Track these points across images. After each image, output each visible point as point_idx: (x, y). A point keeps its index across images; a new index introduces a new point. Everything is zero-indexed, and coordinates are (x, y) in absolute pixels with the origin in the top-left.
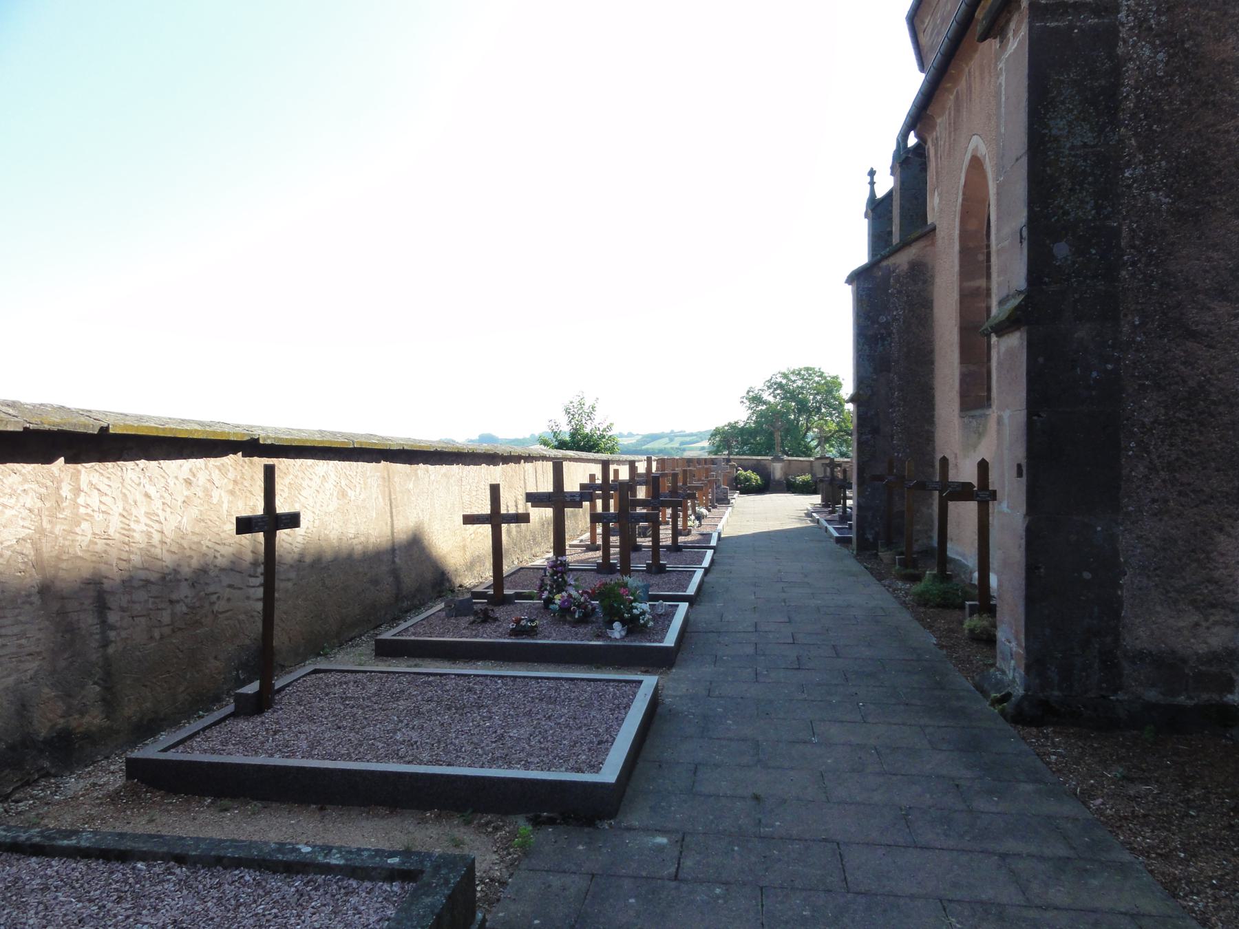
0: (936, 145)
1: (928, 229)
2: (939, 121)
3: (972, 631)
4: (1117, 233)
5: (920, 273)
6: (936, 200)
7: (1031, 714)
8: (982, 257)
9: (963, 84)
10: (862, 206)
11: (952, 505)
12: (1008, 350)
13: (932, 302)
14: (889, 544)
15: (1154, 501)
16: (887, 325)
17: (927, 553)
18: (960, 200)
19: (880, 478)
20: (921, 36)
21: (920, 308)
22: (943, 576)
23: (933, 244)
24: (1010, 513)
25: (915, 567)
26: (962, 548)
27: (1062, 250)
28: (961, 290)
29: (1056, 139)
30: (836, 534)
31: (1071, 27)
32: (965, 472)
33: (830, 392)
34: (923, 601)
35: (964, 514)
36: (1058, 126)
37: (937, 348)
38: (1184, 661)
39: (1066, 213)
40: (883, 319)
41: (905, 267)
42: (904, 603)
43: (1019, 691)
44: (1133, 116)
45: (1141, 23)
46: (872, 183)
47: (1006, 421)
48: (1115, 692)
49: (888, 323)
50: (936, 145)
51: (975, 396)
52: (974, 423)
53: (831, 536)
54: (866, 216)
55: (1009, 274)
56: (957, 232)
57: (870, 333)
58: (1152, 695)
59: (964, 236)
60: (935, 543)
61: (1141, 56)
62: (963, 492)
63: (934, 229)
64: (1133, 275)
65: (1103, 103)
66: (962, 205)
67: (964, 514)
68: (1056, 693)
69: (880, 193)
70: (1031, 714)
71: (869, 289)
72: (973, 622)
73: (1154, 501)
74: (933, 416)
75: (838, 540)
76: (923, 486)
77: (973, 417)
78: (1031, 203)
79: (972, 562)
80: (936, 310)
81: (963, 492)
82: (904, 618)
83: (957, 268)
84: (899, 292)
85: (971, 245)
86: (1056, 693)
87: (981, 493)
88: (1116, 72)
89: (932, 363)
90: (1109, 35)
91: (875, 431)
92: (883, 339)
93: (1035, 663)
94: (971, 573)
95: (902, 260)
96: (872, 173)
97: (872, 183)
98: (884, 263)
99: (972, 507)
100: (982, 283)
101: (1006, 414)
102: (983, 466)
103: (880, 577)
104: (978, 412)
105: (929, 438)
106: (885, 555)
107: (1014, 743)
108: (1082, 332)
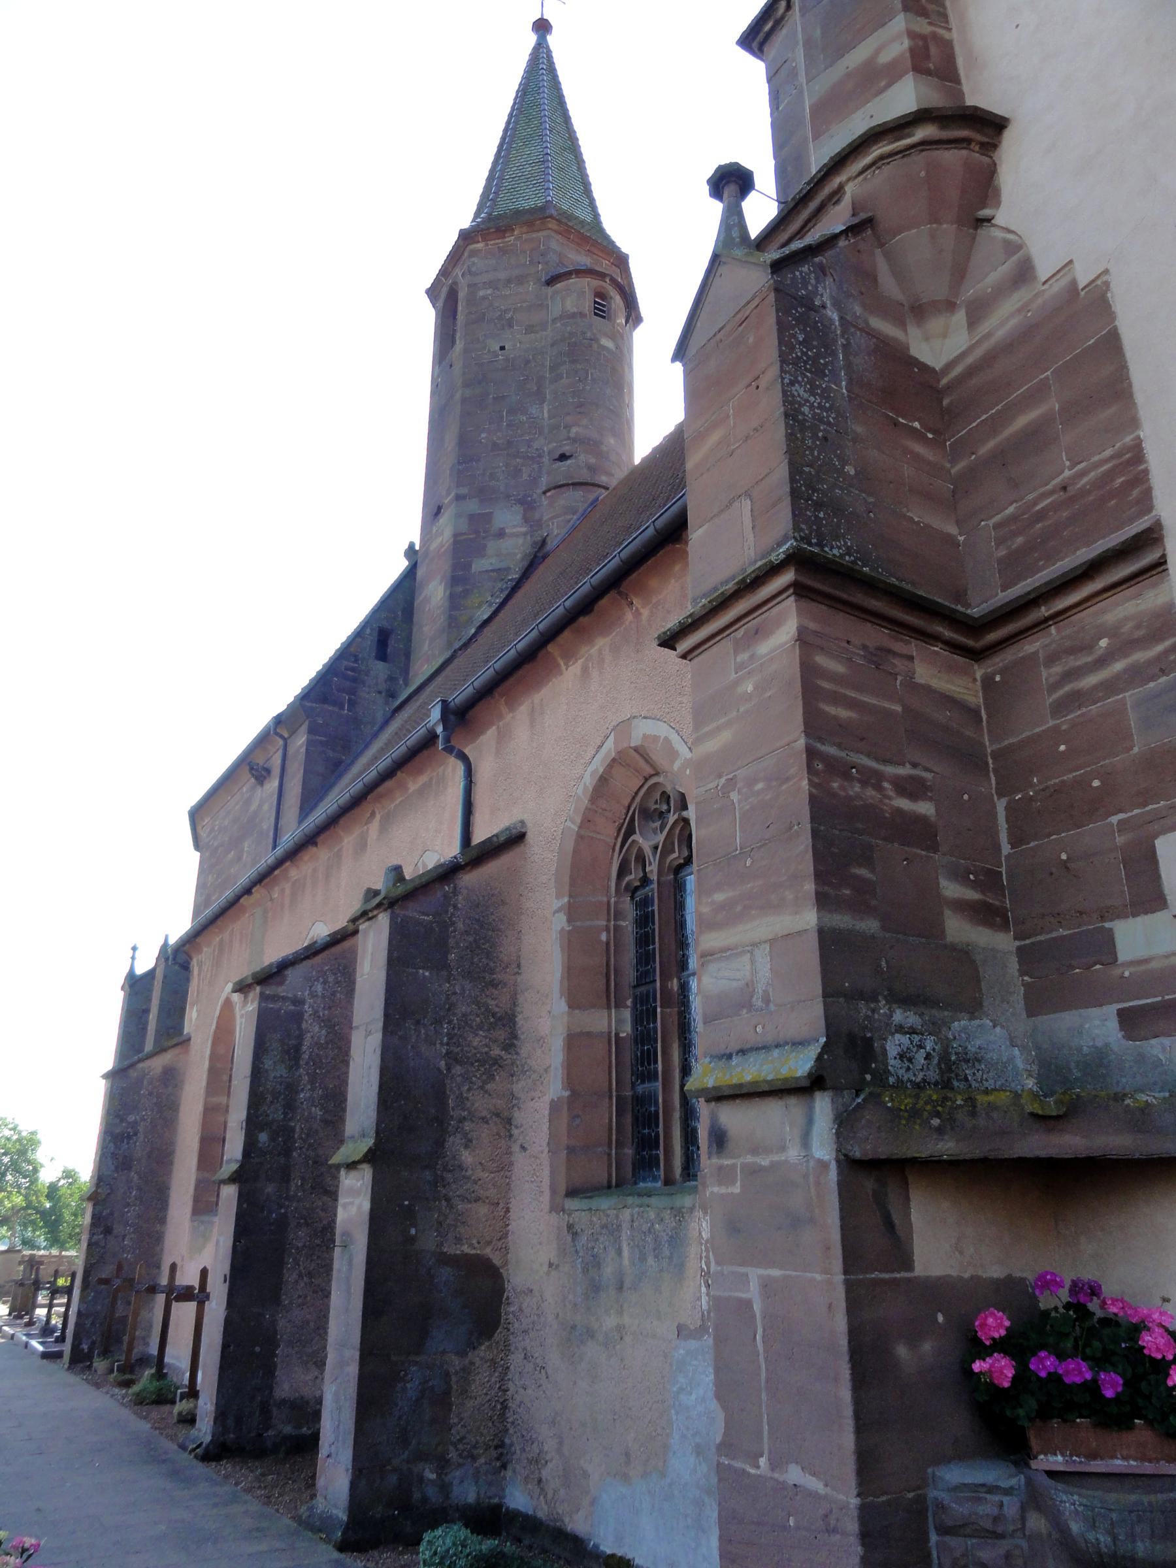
0: (200, 965)
1: (182, 1039)
2: (205, 949)
3: (180, 1414)
4: (293, 1130)
5: (171, 1077)
6: (194, 1014)
7: (213, 1454)
8: (225, 1078)
9: (226, 936)
10: (121, 979)
11: (174, 1304)
12: (230, 1193)
13: (179, 1105)
14: (105, 1353)
15: (299, 1297)
16: (134, 1124)
17: (144, 1361)
18: (214, 1027)
19: (106, 1281)
20: (199, 828)
21: (166, 1111)
22: (160, 1375)
23: (187, 1051)
24: (216, 1309)
25: (132, 1372)
26: (178, 1356)
27: (263, 1137)
28: (206, 1104)
29: (267, 1071)
30: (40, 1348)
31: (280, 1009)
32: (189, 1277)
33: (22, 1152)
34: (140, 1401)
35: (184, 1312)
36: (268, 1064)
37: (176, 1161)
38: (307, 1403)
39: (267, 1115)
40: (131, 1118)
41: (159, 1070)
42: (122, 1404)
43: (208, 1438)
44: (307, 1064)
45: (316, 1012)
46: (133, 958)
47: (221, 1243)
48: (267, 1430)
49: (136, 1122)
50: (200, 965)
51: (203, 1206)
52: (202, 1228)
53: (34, 1351)
54: (123, 988)
55: (234, 1148)
56: (208, 1052)
57: (118, 1131)
58: (288, 1429)
59: (213, 1057)
60: (154, 1351)
61: (314, 1031)
62: (186, 1294)
63: (189, 1039)
64: (300, 1155)
65: (293, 1054)
66: (215, 1032)
67: (184, 1312)
68: (232, 1436)
69: (140, 970)
70: (213, 1454)
71: (123, 1088)
72: (181, 1406)
73: (299, 1297)
74: (165, 1217)
75: (45, 1356)
76: (153, 1289)
77: (202, 1222)
78: (249, 1108)
79: (185, 1364)
80: (181, 1114)
81: (186, 1294)
82: (126, 1415)
83: (204, 1083)
84: (150, 1094)
85: (219, 1065)
86: (232, 1436)
87: (198, 1295)
88: (300, 1037)
89: (172, 1163)
90: (298, 1017)
91: (108, 1231)
92: (129, 1137)
93: (221, 1416)
94: (183, 1374)
95: (157, 1064)
96: (134, 949)
97: (133, 958)
98: (141, 1065)
99: (192, 1306)
100: (223, 1100)
101: (222, 1239)
102: (204, 1273)
103: (97, 1385)
104: (205, 1218)
105: (158, 1239)
106: (100, 1365)
107: (201, 1469)
108: (270, 1189)
